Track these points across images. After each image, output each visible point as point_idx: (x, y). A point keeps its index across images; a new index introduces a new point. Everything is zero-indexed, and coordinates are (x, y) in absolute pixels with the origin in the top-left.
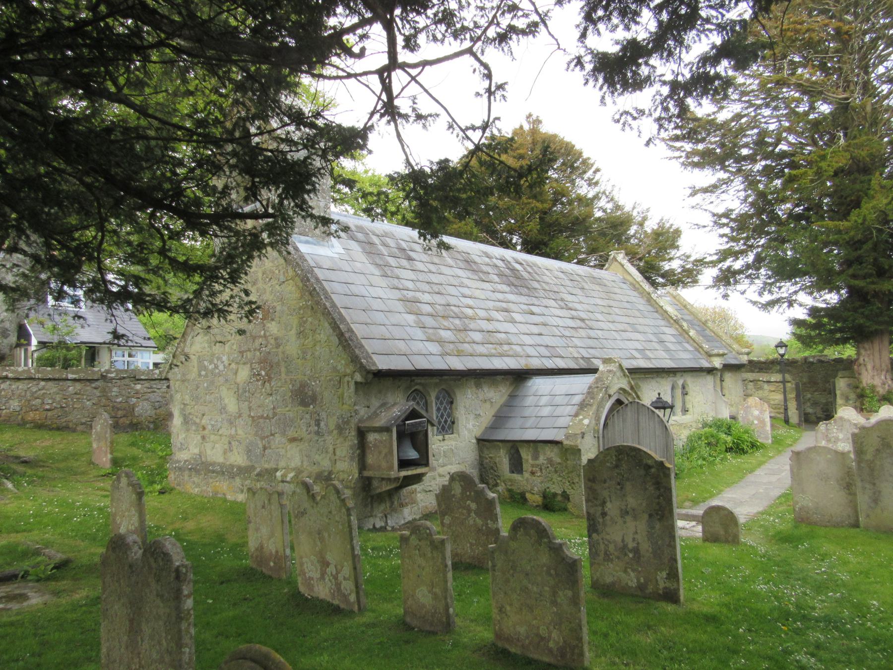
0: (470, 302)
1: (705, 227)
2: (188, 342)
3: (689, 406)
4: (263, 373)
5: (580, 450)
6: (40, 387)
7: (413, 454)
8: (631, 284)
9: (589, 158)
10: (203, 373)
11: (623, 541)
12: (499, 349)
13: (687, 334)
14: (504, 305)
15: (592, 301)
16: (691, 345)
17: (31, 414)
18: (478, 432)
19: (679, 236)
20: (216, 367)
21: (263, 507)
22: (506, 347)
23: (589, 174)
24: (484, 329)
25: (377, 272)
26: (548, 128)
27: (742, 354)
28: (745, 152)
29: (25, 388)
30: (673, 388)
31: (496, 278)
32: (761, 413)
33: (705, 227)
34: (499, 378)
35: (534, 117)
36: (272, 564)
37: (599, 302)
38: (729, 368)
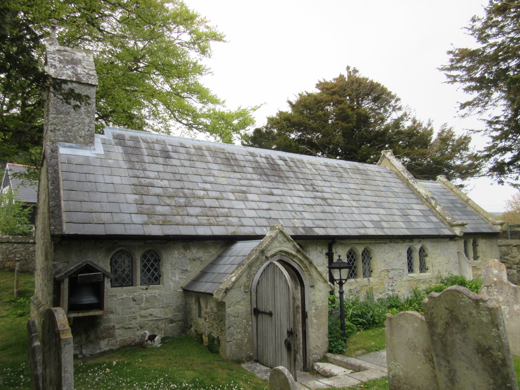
0: (208, 186)
1: (479, 131)
3: (428, 265)
5: (224, 303)
6: (14, 247)
7: (89, 299)
8: (396, 173)
9: (391, 92)
12: (212, 220)
13: (435, 209)
14: (244, 189)
15: (346, 186)
16: (438, 218)
17: (8, 263)
18: (184, 283)
19: (469, 141)
22: (221, 219)
23: (393, 102)
24: (208, 205)
25: (124, 165)
26: (362, 74)
27: (496, 224)
29: (6, 248)
30: (410, 252)
31: (250, 170)
32: (499, 272)
33: (479, 131)
34: (208, 242)
35: (351, 70)
37: (352, 186)
38: (467, 236)
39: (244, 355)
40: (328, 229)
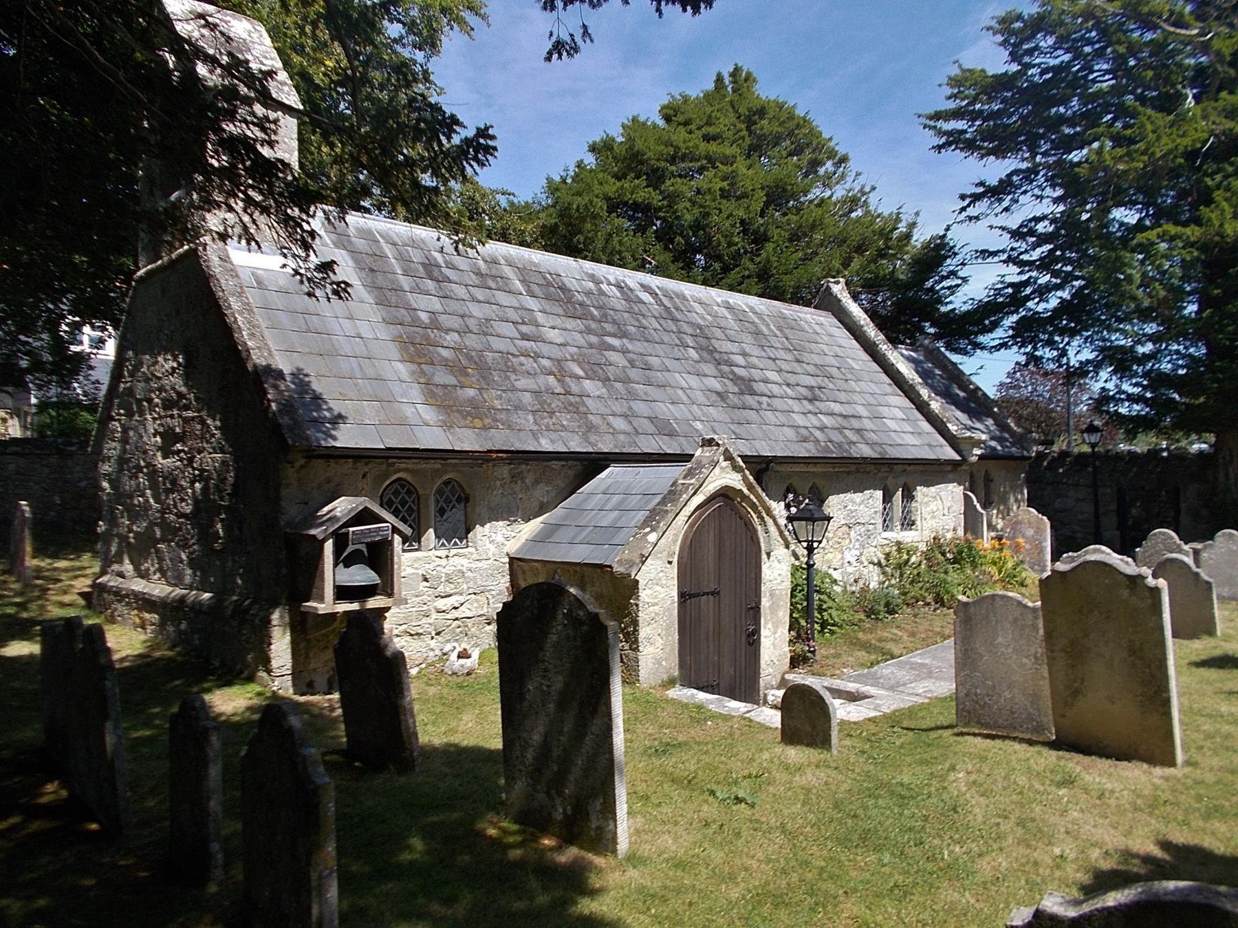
40: (756, 443)
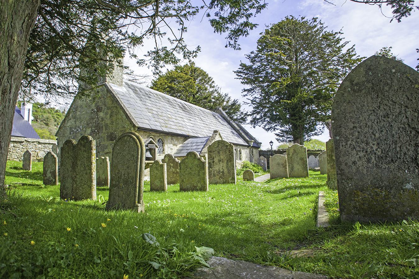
2: (66, 122)
4: (96, 131)
10: (72, 133)
11: (219, 169)
20: (77, 130)
21: (101, 164)
22: (181, 128)
28: (261, 79)
36: (103, 183)
39: (189, 186)
